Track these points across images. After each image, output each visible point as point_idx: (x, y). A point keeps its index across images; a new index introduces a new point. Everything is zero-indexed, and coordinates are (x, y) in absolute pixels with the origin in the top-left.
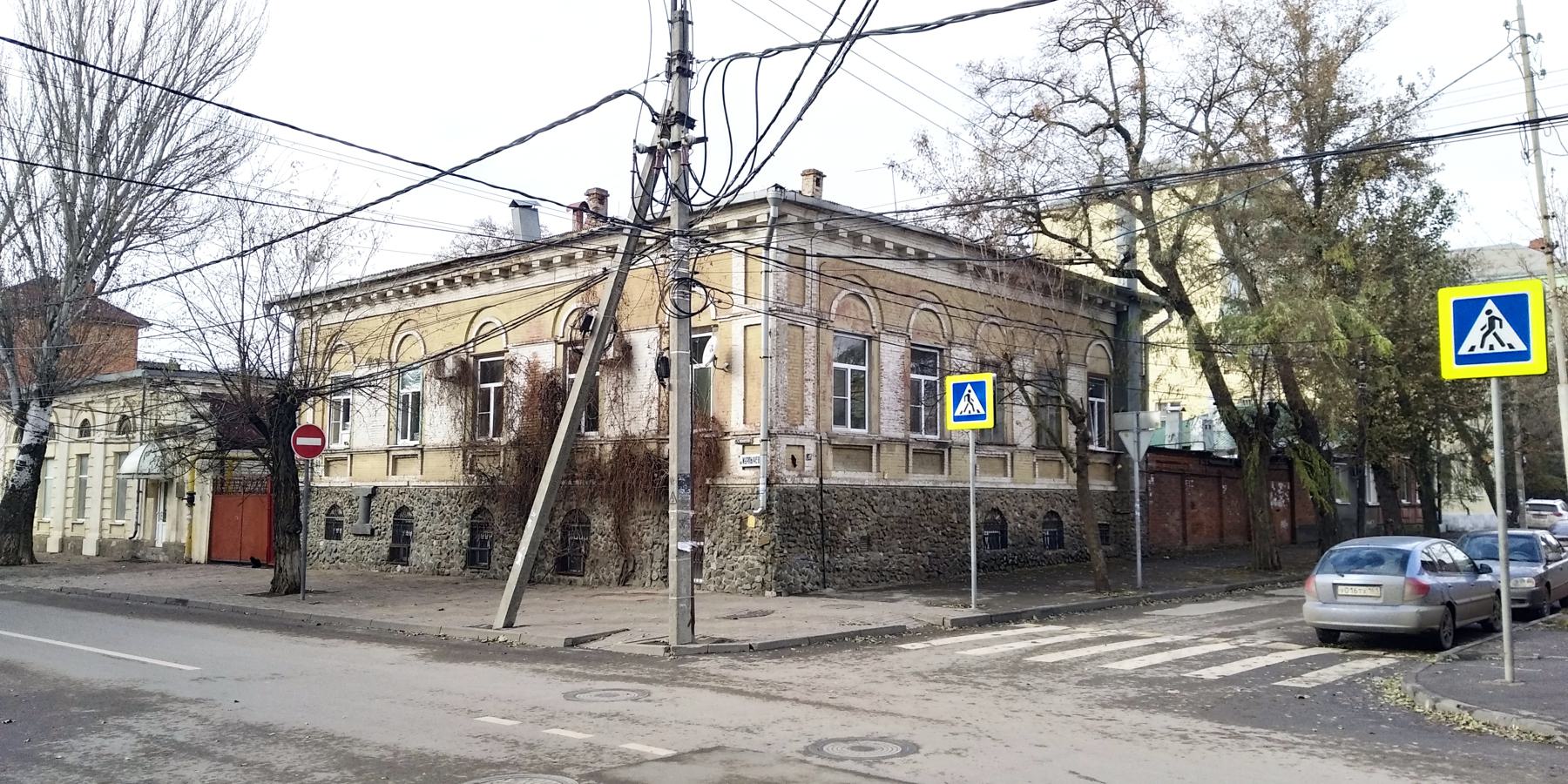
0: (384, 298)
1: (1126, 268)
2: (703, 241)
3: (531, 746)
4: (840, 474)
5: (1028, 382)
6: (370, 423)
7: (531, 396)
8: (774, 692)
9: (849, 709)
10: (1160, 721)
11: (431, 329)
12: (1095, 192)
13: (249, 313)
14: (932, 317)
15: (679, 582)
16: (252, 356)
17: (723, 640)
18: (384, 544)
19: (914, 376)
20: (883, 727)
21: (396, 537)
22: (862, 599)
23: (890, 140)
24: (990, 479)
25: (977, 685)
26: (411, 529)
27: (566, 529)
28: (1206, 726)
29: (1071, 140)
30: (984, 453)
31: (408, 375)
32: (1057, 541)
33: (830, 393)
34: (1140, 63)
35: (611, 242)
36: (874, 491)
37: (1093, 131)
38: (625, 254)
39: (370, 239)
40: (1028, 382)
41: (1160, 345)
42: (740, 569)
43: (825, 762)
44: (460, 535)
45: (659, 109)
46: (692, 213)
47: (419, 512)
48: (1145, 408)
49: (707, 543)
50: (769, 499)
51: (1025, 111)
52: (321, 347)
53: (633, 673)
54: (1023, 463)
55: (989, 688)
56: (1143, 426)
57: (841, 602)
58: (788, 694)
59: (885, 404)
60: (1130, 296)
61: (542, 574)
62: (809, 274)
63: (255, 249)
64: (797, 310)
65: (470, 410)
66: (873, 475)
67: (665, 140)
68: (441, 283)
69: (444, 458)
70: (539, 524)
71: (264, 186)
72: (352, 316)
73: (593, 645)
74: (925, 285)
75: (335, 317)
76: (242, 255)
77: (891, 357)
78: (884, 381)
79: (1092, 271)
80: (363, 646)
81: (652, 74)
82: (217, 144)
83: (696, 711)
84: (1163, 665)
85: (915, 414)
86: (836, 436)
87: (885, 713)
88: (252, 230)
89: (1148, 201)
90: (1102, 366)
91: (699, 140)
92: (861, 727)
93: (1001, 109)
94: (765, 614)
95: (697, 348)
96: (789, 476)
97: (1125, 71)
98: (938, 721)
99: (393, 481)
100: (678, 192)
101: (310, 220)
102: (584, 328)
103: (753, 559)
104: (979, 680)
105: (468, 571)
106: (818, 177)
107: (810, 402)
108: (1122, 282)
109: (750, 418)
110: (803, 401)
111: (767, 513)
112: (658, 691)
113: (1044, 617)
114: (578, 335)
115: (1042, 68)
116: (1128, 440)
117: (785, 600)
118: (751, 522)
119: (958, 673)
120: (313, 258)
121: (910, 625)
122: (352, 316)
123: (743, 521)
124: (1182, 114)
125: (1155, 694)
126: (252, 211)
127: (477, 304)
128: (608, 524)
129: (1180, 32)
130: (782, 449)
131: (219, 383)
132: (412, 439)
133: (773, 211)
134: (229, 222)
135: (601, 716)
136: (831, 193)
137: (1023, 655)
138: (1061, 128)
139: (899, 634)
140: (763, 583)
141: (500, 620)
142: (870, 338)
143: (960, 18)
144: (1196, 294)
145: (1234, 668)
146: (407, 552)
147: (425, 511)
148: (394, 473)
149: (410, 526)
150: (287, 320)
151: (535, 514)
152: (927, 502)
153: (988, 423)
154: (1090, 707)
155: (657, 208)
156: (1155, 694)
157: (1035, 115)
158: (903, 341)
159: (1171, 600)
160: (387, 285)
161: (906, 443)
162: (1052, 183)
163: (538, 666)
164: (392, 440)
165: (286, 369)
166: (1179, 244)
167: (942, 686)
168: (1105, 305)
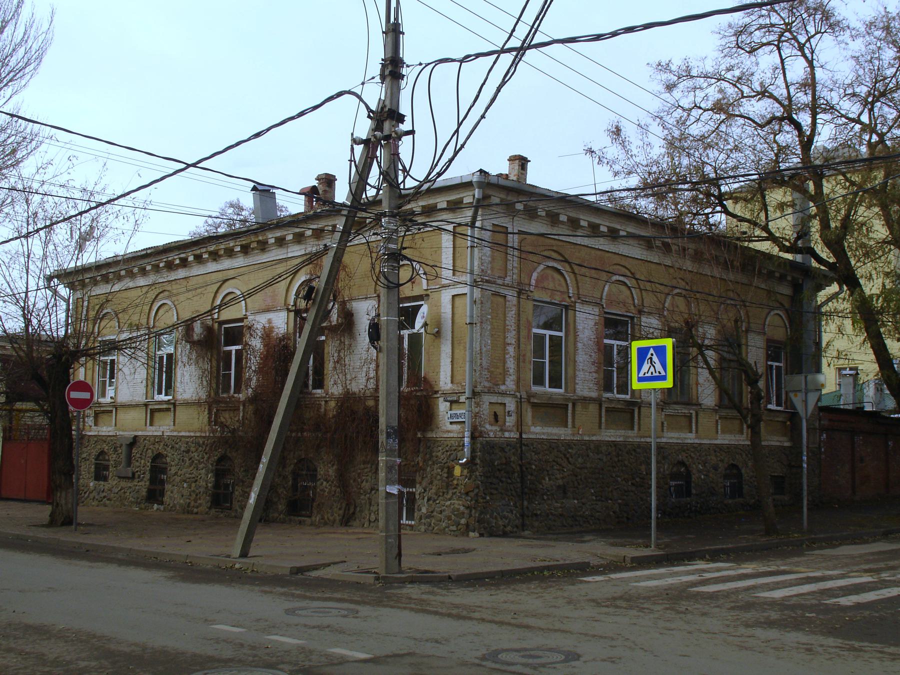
0: (143, 272)
1: (800, 243)
2: (411, 220)
3: (253, 648)
4: (538, 429)
5: (708, 347)
6: (130, 382)
7: (265, 358)
8: (465, 613)
9: (527, 627)
10: (793, 637)
11: (182, 298)
12: (772, 177)
13: (32, 285)
14: (623, 288)
15: (387, 521)
16: (35, 322)
17: (426, 572)
18: (143, 486)
19: (606, 341)
20: (554, 640)
21: (153, 480)
22: (556, 540)
23: (576, 131)
24: (676, 435)
25: (642, 609)
26: (165, 473)
27: (296, 475)
28: (831, 641)
29: (750, 130)
30: (669, 411)
31: (164, 338)
32: (737, 490)
33: (530, 357)
34: (810, 63)
35: (330, 222)
36: (569, 444)
37: (769, 122)
38: (343, 232)
39: (132, 220)
40: (708, 347)
41: (830, 314)
42: (446, 513)
43: (497, 666)
44: (207, 479)
45: (374, 107)
46: (401, 196)
47: (172, 458)
48: (818, 370)
49: (418, 490)
50: (473, 451)
51: (709, 105)
52: (92, 314)
53: (346, 596)
54: (707, 421)
55: (651, 611)
56: (810, 387)
57: (535, 542)
58: (476, 615)
59: (580, 366)
60: (804, 270)
61: (276, 515)
62: (510, 251)
63: (38, 231)
64: (500, 281)
65: (214, 369)
66: (569, 431)
67: (378, 133)
68: (191, 258)
69: (193, 412)
70: (269, 469)
71: (45, 178)
72: (117, 288)
73: (314, 574)
74: (617, 259)
75: (101, 289)
76: (27, 236)
77: (586, 322)
78: (580, 345)
79: (765, 246)
80: (122, 568)
81: (368, 77)
82: (10, 141)
83: (396, 626)
84: (808, 594)
85: (608, 377)
86: (535, 395)
87: (556, 631)
88: (35, 214)
89: (819, 186)
90: (780, 334)
91: (408, 133)
92: (534, 640)
93: (686, 103)
94: (466, 551)
95: (409, 316)
96: (491, 430)
97: (797, 69)
98: (601, 637)
99: (152, 431)
100: (389, 178)
101: (83, 206)
102: (307, 297)
103: (458, 504)
104: (645, 606)
105: (213, 510)
106: (522, 162)
107: (511, 364)
108: (799, 258)
109: (458, 378)
110: (505, 362)
111: (471, 462)
112: (364, 610)
113: (714, 556)
114: (302, 304)
115: (723, 67)
116: (797, 400)
117: (486, 540)
118: (457, 471)
119: (628, 600)
120: (84, 239)
121: (594, 561)
122: (117, 288)
123: (450, 471)
124: (852, 108)
125: (793, 616)
126: (36, 198)
127: (221, 276)
128: (332, 472)
129: (846, 36)
130: (486, 406)
131: (9, 346)
132: (166, 395)
133: (477, 193)
134: (17, 208)
135: (314, 627)
136: (535, 177)
137: (688, 587)
138: (741, 121)
139: (584, 569)
140: (467, 525)
141: (237, 551)
142: (567, 307)
143: (630, 30)
144: (862, 270)
145: (871, 596)
146: (162, 494)
147: (177, 457)
148: (151, 425)
149: (164, 471)
150: (63, 291)
151: (265, 460)
152: (618, 455)
153: (668, 384)
154: (735, 627)
155: (371, 192)
156: (793, 616)
157: (718, 107)
158: (596, 310)
159: (832, 542)
160: (146, 261)
161: (599, 402)
162: (735, 168)
163: (267, 589)
164: (149, 395)
165: (62, 333)
166: (847, 224)
167: (611, 610)
168: (782, 278)
